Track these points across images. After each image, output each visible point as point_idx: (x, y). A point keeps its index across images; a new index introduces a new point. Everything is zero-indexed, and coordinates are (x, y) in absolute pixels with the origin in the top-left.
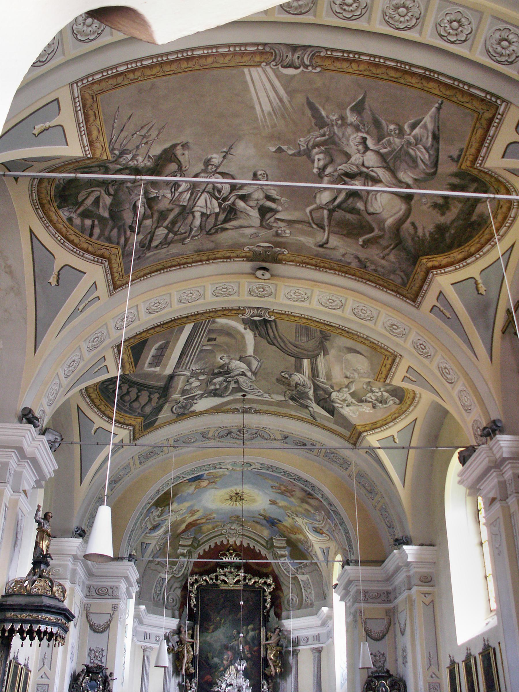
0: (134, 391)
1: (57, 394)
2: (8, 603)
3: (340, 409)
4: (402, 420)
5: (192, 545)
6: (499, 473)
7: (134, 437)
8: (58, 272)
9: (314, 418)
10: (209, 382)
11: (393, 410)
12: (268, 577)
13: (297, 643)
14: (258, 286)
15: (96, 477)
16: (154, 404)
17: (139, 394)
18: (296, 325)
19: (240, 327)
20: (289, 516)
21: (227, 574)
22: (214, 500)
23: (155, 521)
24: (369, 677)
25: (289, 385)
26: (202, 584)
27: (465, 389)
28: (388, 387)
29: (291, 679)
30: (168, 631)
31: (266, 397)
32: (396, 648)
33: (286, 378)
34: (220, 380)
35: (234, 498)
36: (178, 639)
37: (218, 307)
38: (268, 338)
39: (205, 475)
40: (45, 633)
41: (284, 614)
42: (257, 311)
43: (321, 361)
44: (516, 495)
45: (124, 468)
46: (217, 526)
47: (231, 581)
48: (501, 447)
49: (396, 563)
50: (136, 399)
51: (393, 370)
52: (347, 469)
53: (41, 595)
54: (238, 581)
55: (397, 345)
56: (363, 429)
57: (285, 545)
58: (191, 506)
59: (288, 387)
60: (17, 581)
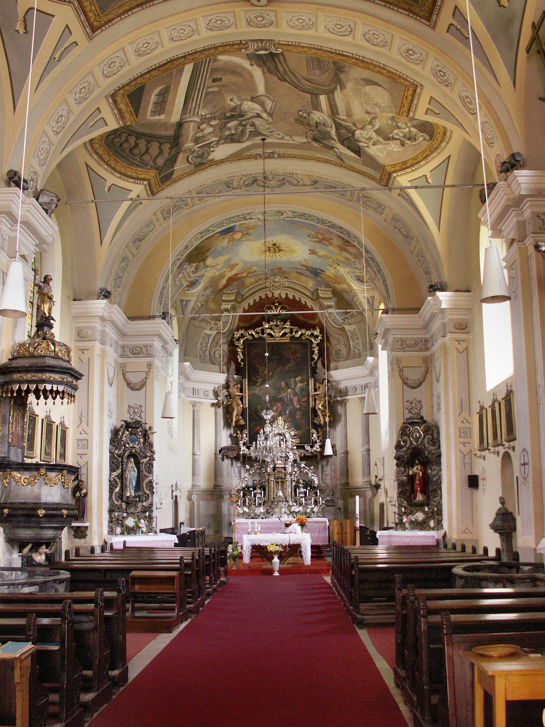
0: (142, 144)
1: (48, 153)
2: (13, 365)
3: (366, 149)
4: (434, 158)
5: (235, 300)
6: (519, 212)
7: (152, 192)
8: (24, 17)
9: (341, 160)
10: (223, 127)
11: (424, 148)
12: (314, 329)
13: (344, 393)
14: (255, 15)
15: (117, 236)
16: (166, 155)
17: (149, 146)
18: (306, 56)
19: (246, 64)
20: (330, 266)
21: (273, 327)
22: (249, 253)
23: (191, 278)
24: (404, 423)
25: (309, 125)
26: (247, 339)
27: (487, 120)
28: (415, 122)
29: (339, 428)
30: (217, 386)
31: (287, 140)
32: (432, 395)
33: (305, 118)
34: (233, 124)
35: (272, 250)
36: (227, 394)
37: (217, 42)
38: (278, 74)
39: (237, 227)
40: (52, 391)
41: (332, 365)
42: (262, 44)
43: (338, 96)
44: (532, 235)
45: (147, 225)
46: (260, 279)
47: (278, 333)
48: (520, 184)
49: (431, 311)
50: (147, 152)
51: (415, 102)
52: (382, 213)
53: (45, 356)
54: (285, 334)
55: (417, 73)
56: (393, 169)
57: (331, 296)
58: (229, 260)
59: (309, 128)
60: (21, 345)
